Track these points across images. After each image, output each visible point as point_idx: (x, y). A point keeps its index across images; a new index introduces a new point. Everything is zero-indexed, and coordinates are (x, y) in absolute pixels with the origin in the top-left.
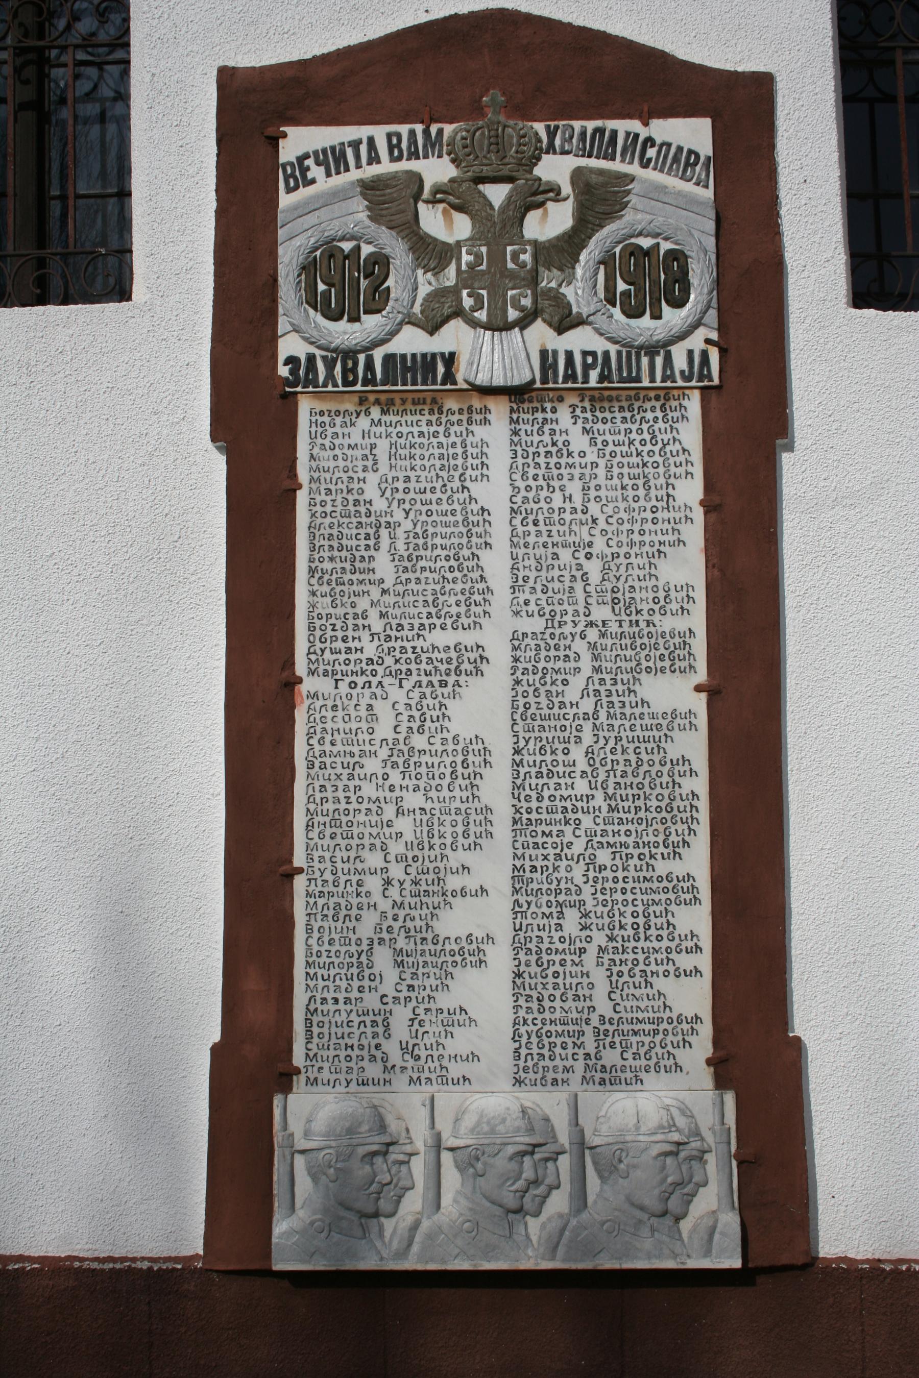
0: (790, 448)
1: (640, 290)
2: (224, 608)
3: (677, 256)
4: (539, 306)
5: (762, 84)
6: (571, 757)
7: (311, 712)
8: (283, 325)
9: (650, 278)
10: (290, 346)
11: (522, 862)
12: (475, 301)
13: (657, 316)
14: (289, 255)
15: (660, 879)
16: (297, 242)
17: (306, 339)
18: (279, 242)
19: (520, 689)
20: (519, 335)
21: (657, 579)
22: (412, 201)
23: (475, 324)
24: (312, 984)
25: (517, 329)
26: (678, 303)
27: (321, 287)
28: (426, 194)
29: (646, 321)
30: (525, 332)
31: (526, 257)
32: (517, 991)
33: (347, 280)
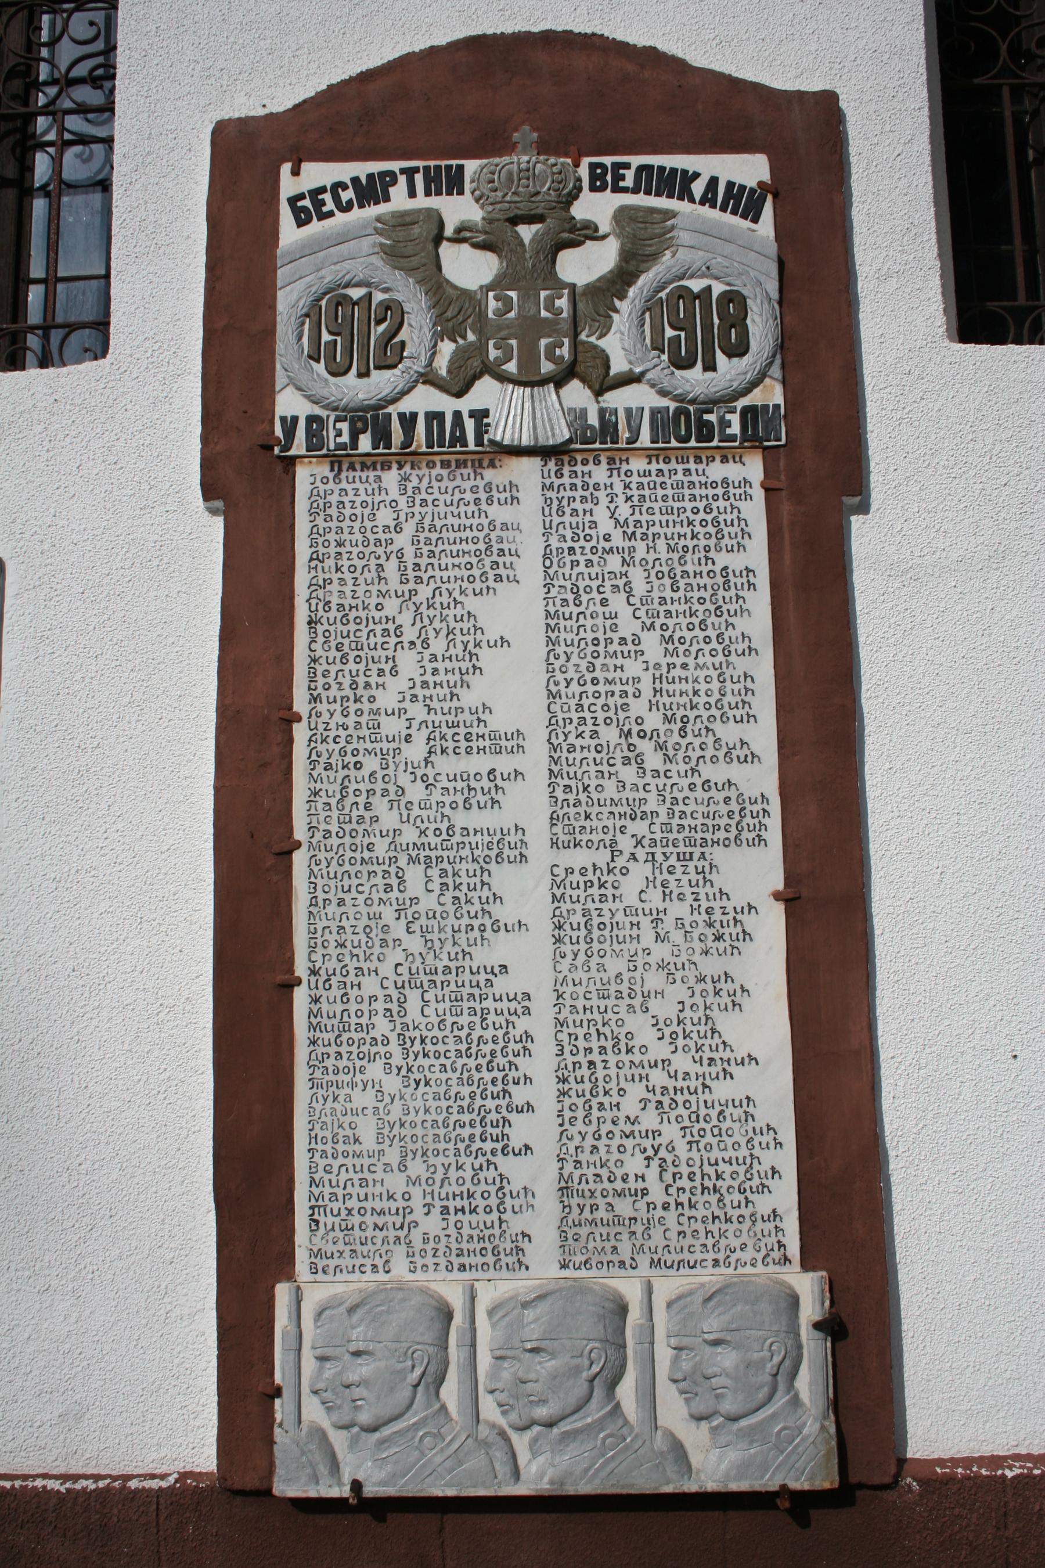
0: (864, 508)
1: (691, 338)
2: (212, 852)
3: (734, 300)
4: (579, 358)
5: (825, 110)
6: (612, 608)
7: (313, 745)
8: (280, 378)
9: (700, 325)
10: (289, 403)
11: (556, 621)
12: (504, 305)
13: (710, 366)
14: (289, 299)
15: (714, 485)
16: (300, 285)
17: (308, 397)
18: (279, 284)
19: (567, 1102)
20: (554, 397)
21: (713, 563)
22: (430, 246)
23: (503, 378)
24: (316, 1191)
25: (552, 385)
26: (738, 350)
27: (326, 337)
28: (449, 232)
29: (696, 373)
30: (562, 392)
31: (563, 303)
32: (548, 581)
33: (353, 330)
